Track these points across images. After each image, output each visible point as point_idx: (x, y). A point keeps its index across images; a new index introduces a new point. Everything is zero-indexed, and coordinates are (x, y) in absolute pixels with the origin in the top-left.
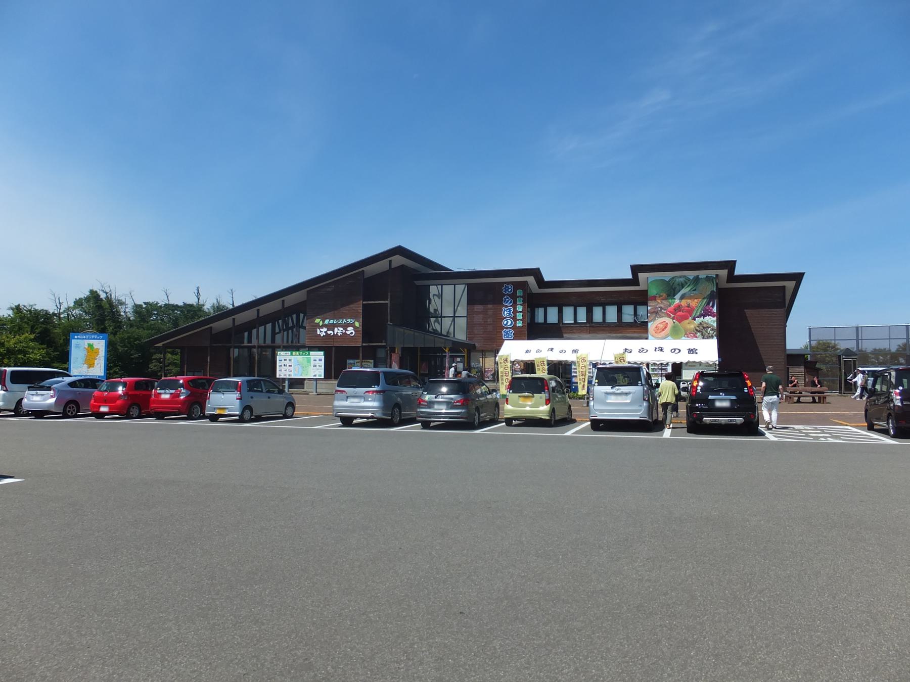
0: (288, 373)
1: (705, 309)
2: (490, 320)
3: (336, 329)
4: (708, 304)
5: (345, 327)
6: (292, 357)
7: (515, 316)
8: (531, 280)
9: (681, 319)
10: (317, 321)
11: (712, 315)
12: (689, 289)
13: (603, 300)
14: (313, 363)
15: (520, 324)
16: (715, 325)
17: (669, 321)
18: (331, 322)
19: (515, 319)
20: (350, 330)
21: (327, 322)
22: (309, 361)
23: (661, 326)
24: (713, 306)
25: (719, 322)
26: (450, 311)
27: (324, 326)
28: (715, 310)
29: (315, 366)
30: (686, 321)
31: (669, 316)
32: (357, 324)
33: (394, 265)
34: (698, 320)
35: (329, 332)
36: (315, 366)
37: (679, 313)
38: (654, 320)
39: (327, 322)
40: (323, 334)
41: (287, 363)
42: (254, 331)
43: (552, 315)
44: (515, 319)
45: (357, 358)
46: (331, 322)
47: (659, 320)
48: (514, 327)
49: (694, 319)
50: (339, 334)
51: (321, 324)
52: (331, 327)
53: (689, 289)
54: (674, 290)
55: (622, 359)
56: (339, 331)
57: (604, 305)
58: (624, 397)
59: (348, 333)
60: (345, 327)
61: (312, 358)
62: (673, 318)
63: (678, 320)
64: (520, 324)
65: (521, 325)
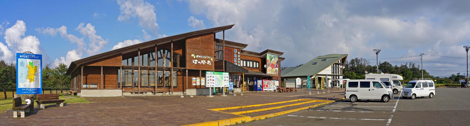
0: (212, 84)
3: (202, 61)
5: (206, 60)
6: (214, 75)
10: (193, 55)
14: (224, 79)
18: (200, 57)
20: (209, 62)
21: (197, 56)
22: (222, 78)
27: (196, 58)
29: (225, 80)
32: (212, 59)
35: (199, 62)
36: (225, 80)
39: (197, 56)
40: (196, 63)
41: (212, 78)
42: (136, 58)
43: (13, 73)
45: (199, 76)
46: (200, 57)
50: (204, 64)
51: (195, 57)
52: (199, 59)
56: (203, 62)
58: (64, 96)
59: (208, 63)
60: (206, 60)
61: (224, 76)
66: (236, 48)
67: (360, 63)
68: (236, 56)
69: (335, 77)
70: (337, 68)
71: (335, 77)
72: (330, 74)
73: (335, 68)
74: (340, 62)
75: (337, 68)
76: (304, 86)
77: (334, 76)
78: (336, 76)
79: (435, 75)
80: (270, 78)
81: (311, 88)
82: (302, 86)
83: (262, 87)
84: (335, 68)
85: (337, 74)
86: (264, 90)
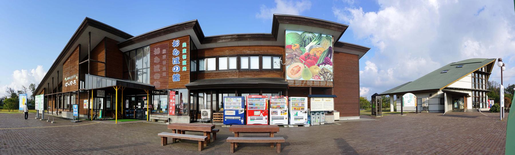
1: (325, 59)
2: (164, 69)
4: (327, 56)
7: (181, 63)
8: (191, 32)
9: (310, 65)
11: (330, 64)
12: (315, 42)
13: (248, 52)
15: (184, 69)
16: (332, 71)
17: (301, 65)
19: (181, 66)
23: (296, 69)
24: (330, 58)
25: (335, 69)
26: (128, 54)
28: (332, 60)
30: (313, 67)
31: (302, 62)
33: (104, 61)
34: (322, 67)
37: (308, 60)
38: (290, 64)
44: (181, 66)
47: (294, 64)
48: (181, 72)
49: (319, 65)
53: (315, 42)
54: (305, 42)
55: (381, 5)
57: (249, 55)
62: (305, 64)
63: (308, 65)
64: (184, 69)
65: (185, 70)
66: (176, 39)
67: (491, 85)
68: (176, 52)
69: (477, 93)
70: (480, 80)
71: (477, 93)
72: (470, 88)
73: (477, 80)
74: (484, 71)
75: (480, 80)
76: (425, 108)
77: (475, 91)
78: (479, 91)
79: (205, 131)
80: (82, 78)
81: (467, 95)
82: (420, 109)
83: (244, 116)
84: (477, 80)
85: (481, 89)
86: (250, 122)
